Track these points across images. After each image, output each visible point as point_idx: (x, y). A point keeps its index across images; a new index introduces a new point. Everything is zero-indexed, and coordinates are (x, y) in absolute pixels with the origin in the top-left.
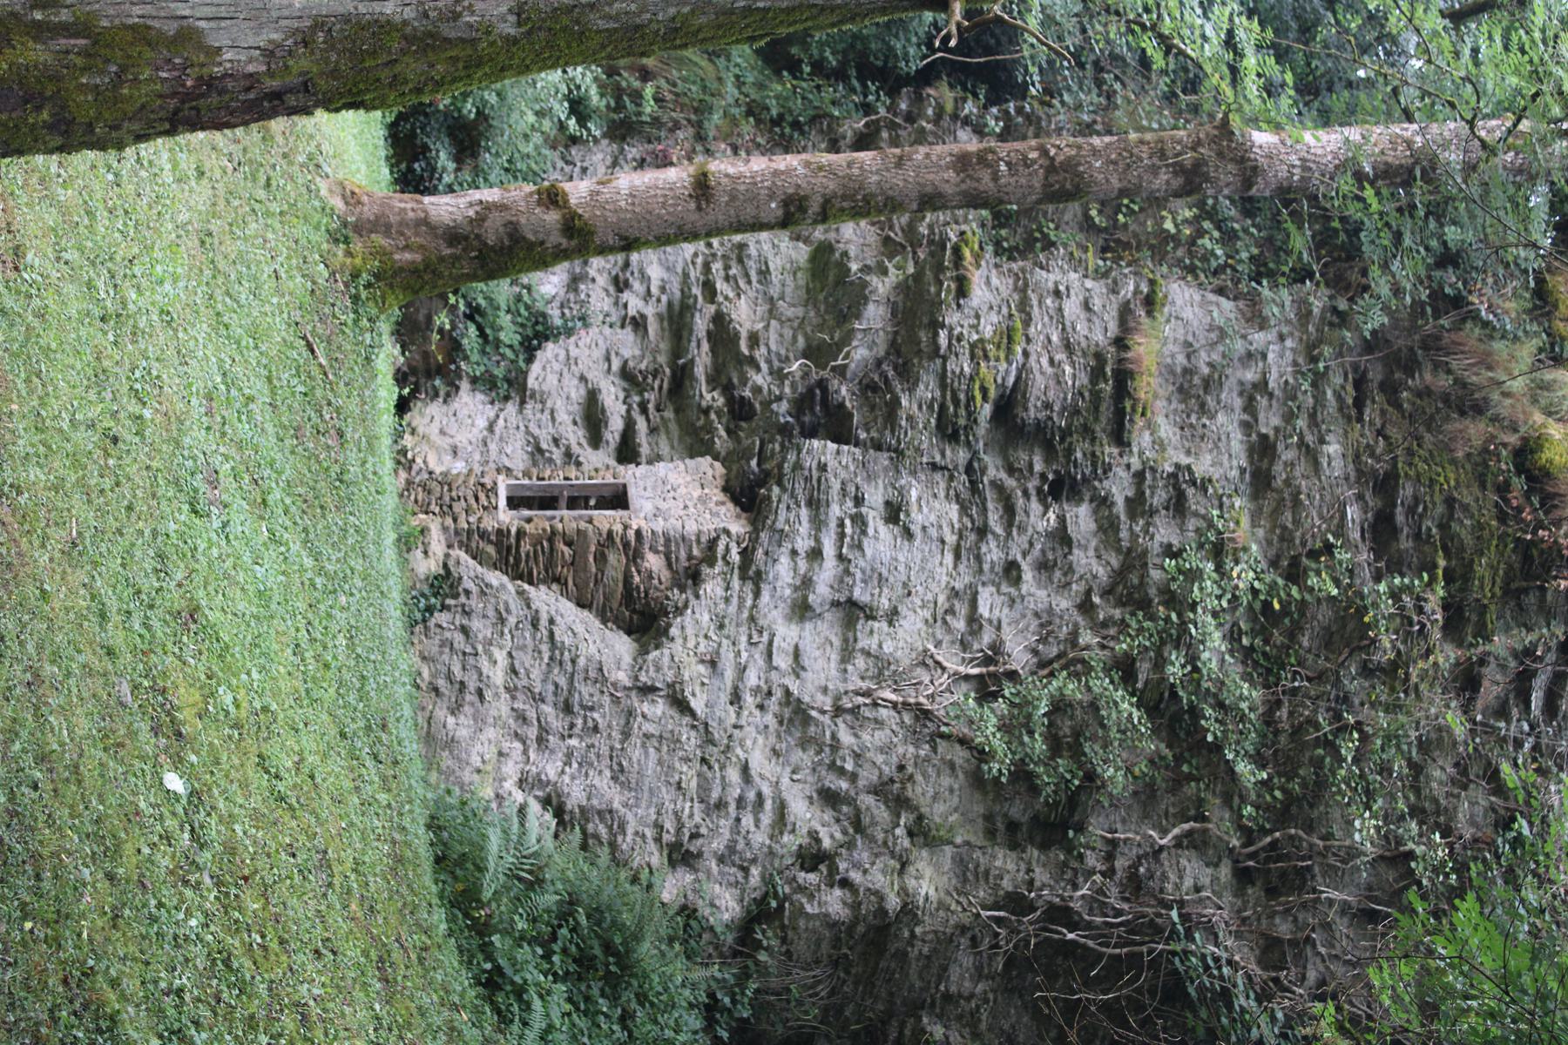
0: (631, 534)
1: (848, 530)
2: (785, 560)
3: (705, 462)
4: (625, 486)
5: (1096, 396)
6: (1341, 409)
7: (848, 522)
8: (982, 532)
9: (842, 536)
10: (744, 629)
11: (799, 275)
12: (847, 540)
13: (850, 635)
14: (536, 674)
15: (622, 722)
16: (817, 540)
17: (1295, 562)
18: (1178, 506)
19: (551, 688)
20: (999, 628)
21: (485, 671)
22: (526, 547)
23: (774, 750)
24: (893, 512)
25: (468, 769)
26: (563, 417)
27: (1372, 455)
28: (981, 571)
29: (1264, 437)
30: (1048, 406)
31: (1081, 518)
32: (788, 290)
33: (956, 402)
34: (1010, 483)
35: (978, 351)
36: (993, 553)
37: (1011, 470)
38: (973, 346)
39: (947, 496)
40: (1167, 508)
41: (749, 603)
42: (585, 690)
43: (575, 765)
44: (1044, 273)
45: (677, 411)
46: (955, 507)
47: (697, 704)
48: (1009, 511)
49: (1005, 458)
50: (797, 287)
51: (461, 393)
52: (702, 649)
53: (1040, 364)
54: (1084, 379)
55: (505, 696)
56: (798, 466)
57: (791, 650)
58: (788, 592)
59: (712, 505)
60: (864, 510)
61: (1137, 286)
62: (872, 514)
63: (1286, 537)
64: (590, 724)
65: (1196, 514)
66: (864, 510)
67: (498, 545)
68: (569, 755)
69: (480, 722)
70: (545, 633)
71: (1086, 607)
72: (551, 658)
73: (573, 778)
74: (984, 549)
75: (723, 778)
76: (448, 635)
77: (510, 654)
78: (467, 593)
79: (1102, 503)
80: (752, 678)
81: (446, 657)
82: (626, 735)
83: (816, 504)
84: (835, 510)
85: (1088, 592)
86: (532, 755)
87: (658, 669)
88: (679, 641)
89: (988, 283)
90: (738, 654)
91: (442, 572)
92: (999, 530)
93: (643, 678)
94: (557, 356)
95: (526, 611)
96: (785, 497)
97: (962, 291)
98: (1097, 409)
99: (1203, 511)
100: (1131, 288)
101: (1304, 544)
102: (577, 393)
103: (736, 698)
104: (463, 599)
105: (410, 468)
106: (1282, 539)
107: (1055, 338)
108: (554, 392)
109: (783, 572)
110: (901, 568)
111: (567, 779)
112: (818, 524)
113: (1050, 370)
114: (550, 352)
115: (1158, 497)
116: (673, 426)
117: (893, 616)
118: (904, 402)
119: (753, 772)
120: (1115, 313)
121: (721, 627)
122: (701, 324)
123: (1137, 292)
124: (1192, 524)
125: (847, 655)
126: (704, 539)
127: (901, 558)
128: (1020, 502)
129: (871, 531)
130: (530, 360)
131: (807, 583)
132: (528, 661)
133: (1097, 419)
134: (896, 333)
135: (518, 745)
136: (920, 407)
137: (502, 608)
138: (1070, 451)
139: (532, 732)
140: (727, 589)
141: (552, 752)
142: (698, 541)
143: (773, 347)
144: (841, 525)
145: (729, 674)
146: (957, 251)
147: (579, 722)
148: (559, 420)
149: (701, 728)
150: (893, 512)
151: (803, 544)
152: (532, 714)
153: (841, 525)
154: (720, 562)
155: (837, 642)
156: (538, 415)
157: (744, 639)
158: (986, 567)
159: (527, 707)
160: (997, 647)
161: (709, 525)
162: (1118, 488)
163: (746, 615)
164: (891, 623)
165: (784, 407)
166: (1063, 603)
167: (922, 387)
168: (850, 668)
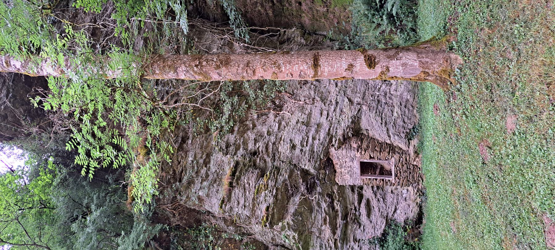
0: (360, 151)
1: (305, 143)
2: (322, 138)
4: (361, 175)
5: (240, 172)
6: (186, 170)
7: (305, 146)
8: (274, 144)
9: (307, 142)
10: (333, 122)
11: (312, 245)
12: (306, 141)
13: (308, 120)
14: (386, 110)
15: (365, 97)
16: (313, 142)
17: (206, 133)
18: (228, 146)
19: (382, 106)
20: (274, 120)
21: (399, 110)
22: (387, 150)
23: (330, 93)
24: (293, 147)
25: (405, 84)
26: (376, 209)
27: (182, 156)
28: (276, 135)
29: (206, 166)
30: (252, 172)
31: (251, 146)
32: (315, 240)
33: (274, 173)
34: (265, 156)
35: (266, 186)
36: (273, 139)
37: (265, 161)
38: (267, 188)
39: (281, 153)
40: (231, 145)
41: (331, 128)
42: (374, 105)
43: (378, 88)
44: (248, 215)
45: (347, 208)
46: (279, 150)
47: (346, 100)
48: (267, 148)
49: (266, 165)
50: (313, 241)
51: (403, 221)
52: (344, 116)
53: (252, 182)
54: (242, 178)
55: (395, 104)
56: (316, 162)
57: (323, 116)
58: (322, 131)
59: (339, 163)
60: (301, 148)
61: (225, 207)
62: (299, 147)
63: (206, 139)
64: (373, 97)
65: (224, 142)
66: (301, 148)
67: (395, 151)
68: (379, 90)
69: (401, 96)
70: (383, 121)
71: (254, 126)
72: (382, 114)
73: (378, 84)
74: (275, 140)
75: (342, 83)
76: (409, 121)
77: (393, 115)
78: (403, 133)
79: (246, 149)
80: (333, 108)
81: (410, 115)
82: (364, 93)
83: (312, 151)
84: (308, 148)
85: (253, 129)
86: (388, 91)
87: (355, 108)
88: (349, 117)
89: (261, 212)
90: (335, 115)
91: (410, 141)
92: (270, 144)
93: (359, 106)
94: (377, 231)
95: (388, 127)
96: (320, 154)
97: (268, 208)
98: (241, 170)
99: (222, 142)
100: (227, 207)
101: (203, 137)
102: (373, 217)
103: (337, 103)
104: (405, 131)
105: (418, 189)
106: (207, 139)
107: (248, 192)
108: (379, 217)
109: (322, 134)
111: (380, 84)
112: (312, 146)
113: (250, 182)
114: (379, 233)
115: (231, 148)
116: (348, 202)
117: (297, 122)
118: (287, 176)
119: (335, 85)
120: (232, 199)
121: (339, 121)
122: (339, 232)
123: (226, 205)
124: (226, 140)
125: (310, 115)
126: (341, 149)
127: (294, 135)
128: (264, 150)
129: (300, 142)
130: (384, 230)
131: (317, 131)
132: (388, 113)
133: (242, 168)
134: (287, 204)
135: (392, 93)
136: (283, 175)
137: (394, 128)
138: (250, 161)
139: (388, 95)
140: (336, 132)
141: (383, 91)
142: (343, 149)
143: (320, 215)
144: (307, 145)
145: (338, 110)
146: (267, 219)
147: (376, 97)
148: (378, 208)
149: (346, 95)
150: (293, 147)
151: (317, 142)
152: (388, 99)
153: (307, 145)
154: (338, 139)
155: (312, 119)
156: (383, 211)
157: (334, 119)
158: (275, 135)
159: (389, 101)
160: (276, 117)
161: (343, 152)
162: (241, 151)
163: (333, 125)
164: (298, 120)
165: (319, 189)
166: (259, 127)
167: (282, 180)
168: (309, 111)
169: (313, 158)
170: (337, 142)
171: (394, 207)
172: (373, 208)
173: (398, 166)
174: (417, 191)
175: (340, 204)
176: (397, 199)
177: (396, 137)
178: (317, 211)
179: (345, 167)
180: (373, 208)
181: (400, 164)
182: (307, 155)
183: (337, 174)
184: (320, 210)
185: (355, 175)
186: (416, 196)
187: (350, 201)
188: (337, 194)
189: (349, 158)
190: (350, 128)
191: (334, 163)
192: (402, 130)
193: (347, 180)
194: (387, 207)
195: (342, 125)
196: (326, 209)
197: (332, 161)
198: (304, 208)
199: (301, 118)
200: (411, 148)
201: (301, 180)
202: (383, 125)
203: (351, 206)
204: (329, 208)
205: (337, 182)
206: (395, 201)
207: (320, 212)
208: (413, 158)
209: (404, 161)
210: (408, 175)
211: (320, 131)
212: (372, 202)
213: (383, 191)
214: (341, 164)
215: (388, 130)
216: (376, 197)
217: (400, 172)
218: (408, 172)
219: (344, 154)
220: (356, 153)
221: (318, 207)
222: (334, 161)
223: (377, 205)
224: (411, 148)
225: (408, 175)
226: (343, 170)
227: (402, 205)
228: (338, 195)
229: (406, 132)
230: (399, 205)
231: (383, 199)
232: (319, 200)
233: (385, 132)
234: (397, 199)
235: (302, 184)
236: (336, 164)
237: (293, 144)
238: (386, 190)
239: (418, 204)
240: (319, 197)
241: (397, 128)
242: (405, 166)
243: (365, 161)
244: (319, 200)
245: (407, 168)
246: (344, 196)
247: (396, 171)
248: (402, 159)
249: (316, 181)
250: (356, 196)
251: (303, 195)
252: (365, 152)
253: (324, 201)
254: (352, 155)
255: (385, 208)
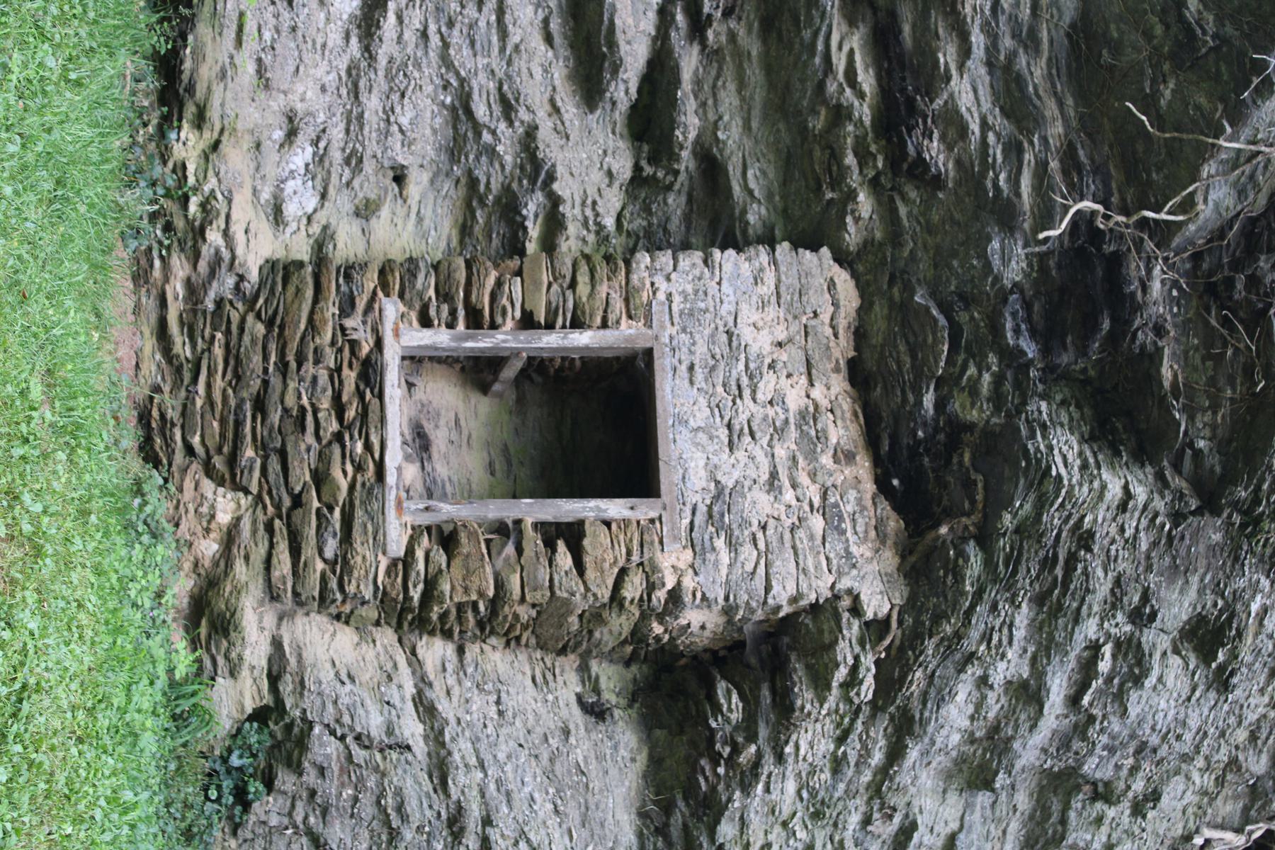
1: (1104, 666)
3: (820, 264)
4: (649, 352)
7: (1107, 650)
10: (860, 802)
13: (1056, 807)
41: (877, 758)
56: (1028, 530)
59: (826, 460)
60: (1148, 637)
66: (1148, 637)
84: (1090, 629)
96: (991, 594)
110: (1188, 736)
116: (755, 74)
121: (817, 815)
127: (1194, 722)
137: (390, 801)
140: (841, 740)
144: (1094, 649)
148: (514, 38)
157: (854, 820)
163: (867, 777)
169: (1048, 563)
170: (841, 674)
171: (386, 50)
172: (555, 26)
173: (359, 468)
174: (199, 233)
175: (831, 88)
176: (355, 121)
177: (374, 722)
178: (1029, 41)
179: (779, 431)
180: (555, 26)
181: (343, 494)
182: (1102, 587)
183: (843, 348)
184: (1007, 42)
185: (701, 349)
186: (212, 183)
187: (742, 85)
188: (854, 179)
189: (746, 523)
190: (731, 762)
191: (863, 468)
192: (329, 788)
193: (763, 305)
194: (435, 40)
195: (791, 786)
196: (947, 55)
197: (882, 485)
198: (1148, 104)
199: (1115, 825)
200: (255, 651)
201: (1166, 373)
202: (474, 812)
203: (732, 36)
204: (927, 52)
205: (843, 278)
206: (373, 104)
207: (1004, 28)
208: (239, 567)
209: (311, 531)
210: (275, 381)
211: (972, 740)
212: (559, 73)
213: (473, 182)
214: (812, 456)
215: (440, 771)
216: (531, 132)
217: (339, 407)
218: (275, 417)
219: (784, 566)
220: (689, 582)
221: (1019, 81)
222: (869, 487)
223: (520, 63)
224: (255, 651)
225: (275, 381)
226: (795, 399)
227: (320, 72)
228: (844, 171)
229: (300, 772)
230: (343, 65)
231: (469, 113)
232: (1014, 150)
233: (461, 750)
234: (355, 121)
235: (1159, 330)
236: (850, 457)
237: (1206, 655)
238: (447, 186)
239: (190, 110)
240: (1015, 182)
241: (367, 800)
242: (301, 475)
243: (615, 508)
244: (1014, 150)
245: (283, 454)
246: (786, 138)
247: (373, 416)
248: (331, 547)
249: (1030, 349)
250: (689, 124)
251: (1163, 233)
252: (616, 597)
253: (963, 131)
254: (725, 558)
255: (456, 37)
